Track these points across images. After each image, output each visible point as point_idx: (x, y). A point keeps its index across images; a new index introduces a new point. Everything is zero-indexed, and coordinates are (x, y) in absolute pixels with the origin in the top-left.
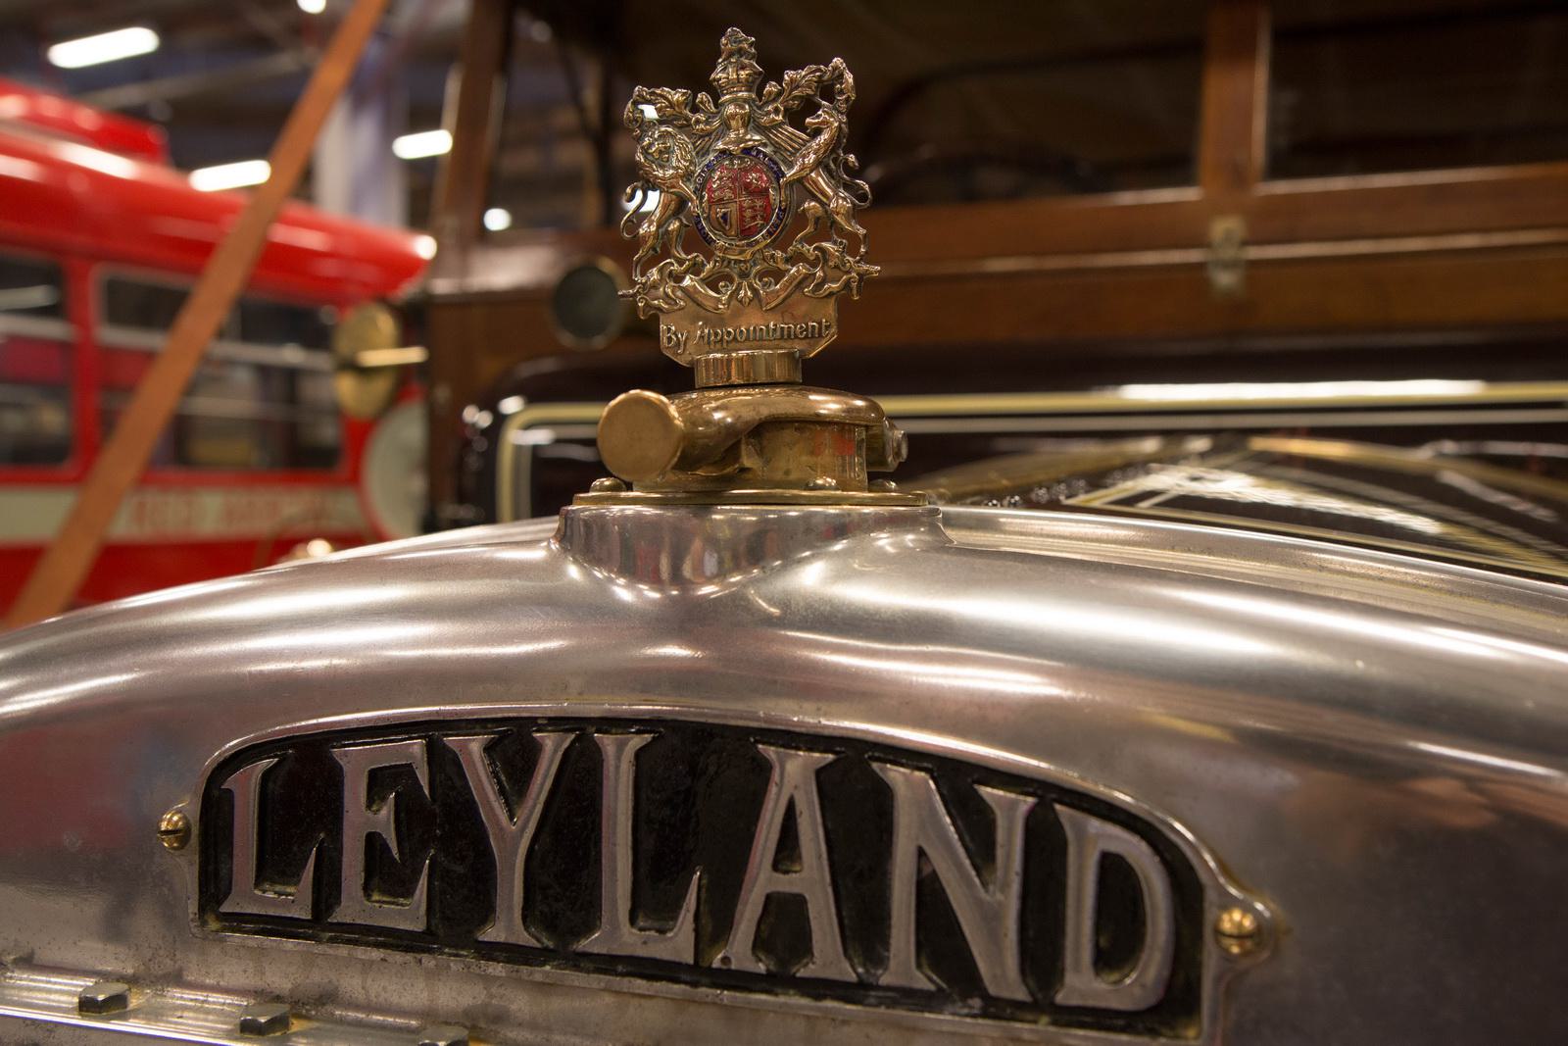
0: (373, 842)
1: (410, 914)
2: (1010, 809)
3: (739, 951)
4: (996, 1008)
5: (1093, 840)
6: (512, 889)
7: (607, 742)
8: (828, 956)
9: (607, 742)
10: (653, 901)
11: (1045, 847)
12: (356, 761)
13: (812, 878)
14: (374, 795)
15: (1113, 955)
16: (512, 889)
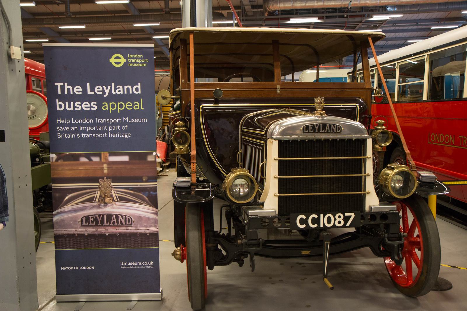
0: (311, 129)
1: (313, 131)
2: (124, 216)
3: (112, 224)
4: (335, 132)
5: (127, 217)
6: (100, 222)
7: (104, 215)
8: (329, 131)
9: (104, 215)
10: (107, 222)
11: (126, 218)
12: (90, 217)
13: (329, 129)
14: (92, 218)
15: (129, 222)
16: (100, 222)
